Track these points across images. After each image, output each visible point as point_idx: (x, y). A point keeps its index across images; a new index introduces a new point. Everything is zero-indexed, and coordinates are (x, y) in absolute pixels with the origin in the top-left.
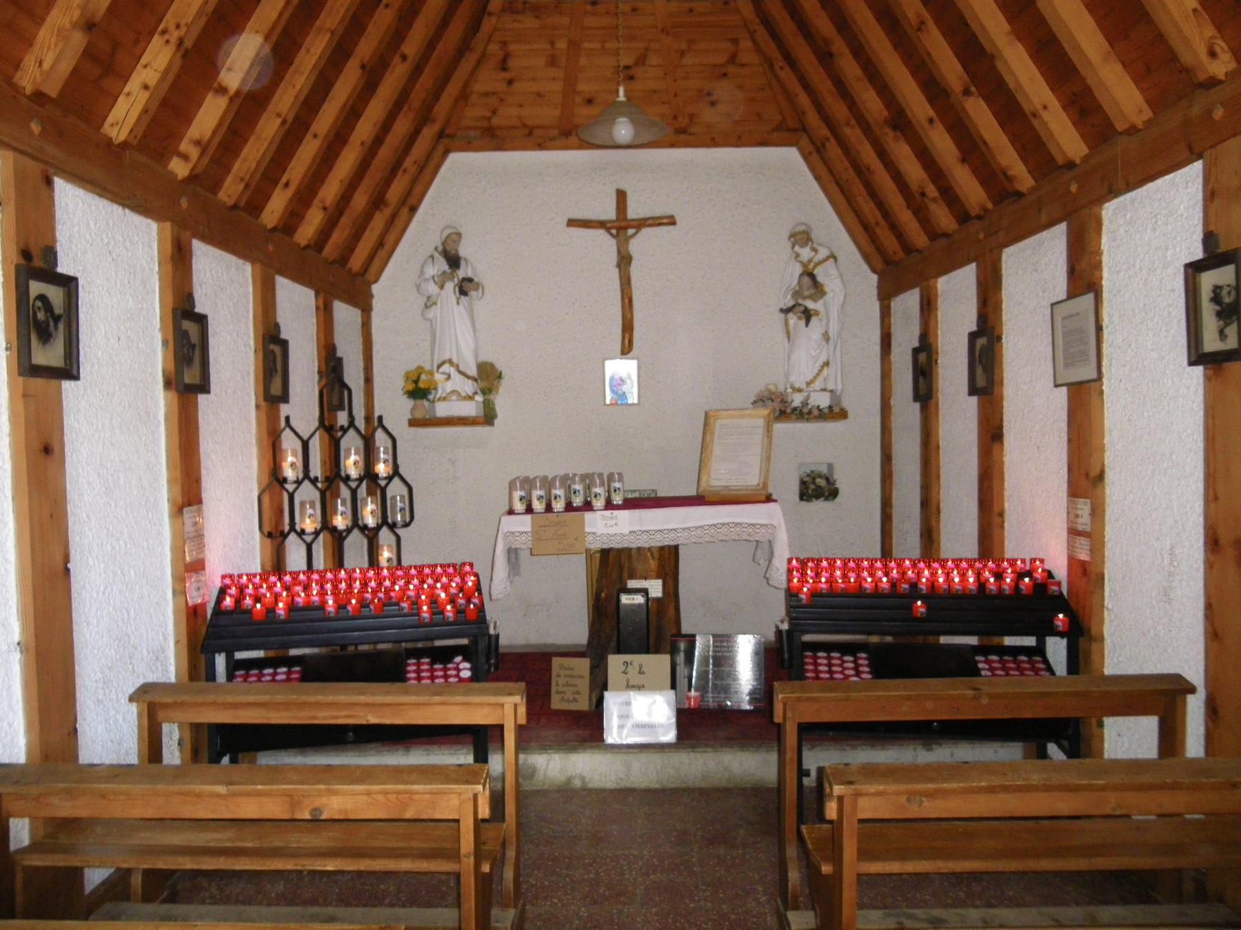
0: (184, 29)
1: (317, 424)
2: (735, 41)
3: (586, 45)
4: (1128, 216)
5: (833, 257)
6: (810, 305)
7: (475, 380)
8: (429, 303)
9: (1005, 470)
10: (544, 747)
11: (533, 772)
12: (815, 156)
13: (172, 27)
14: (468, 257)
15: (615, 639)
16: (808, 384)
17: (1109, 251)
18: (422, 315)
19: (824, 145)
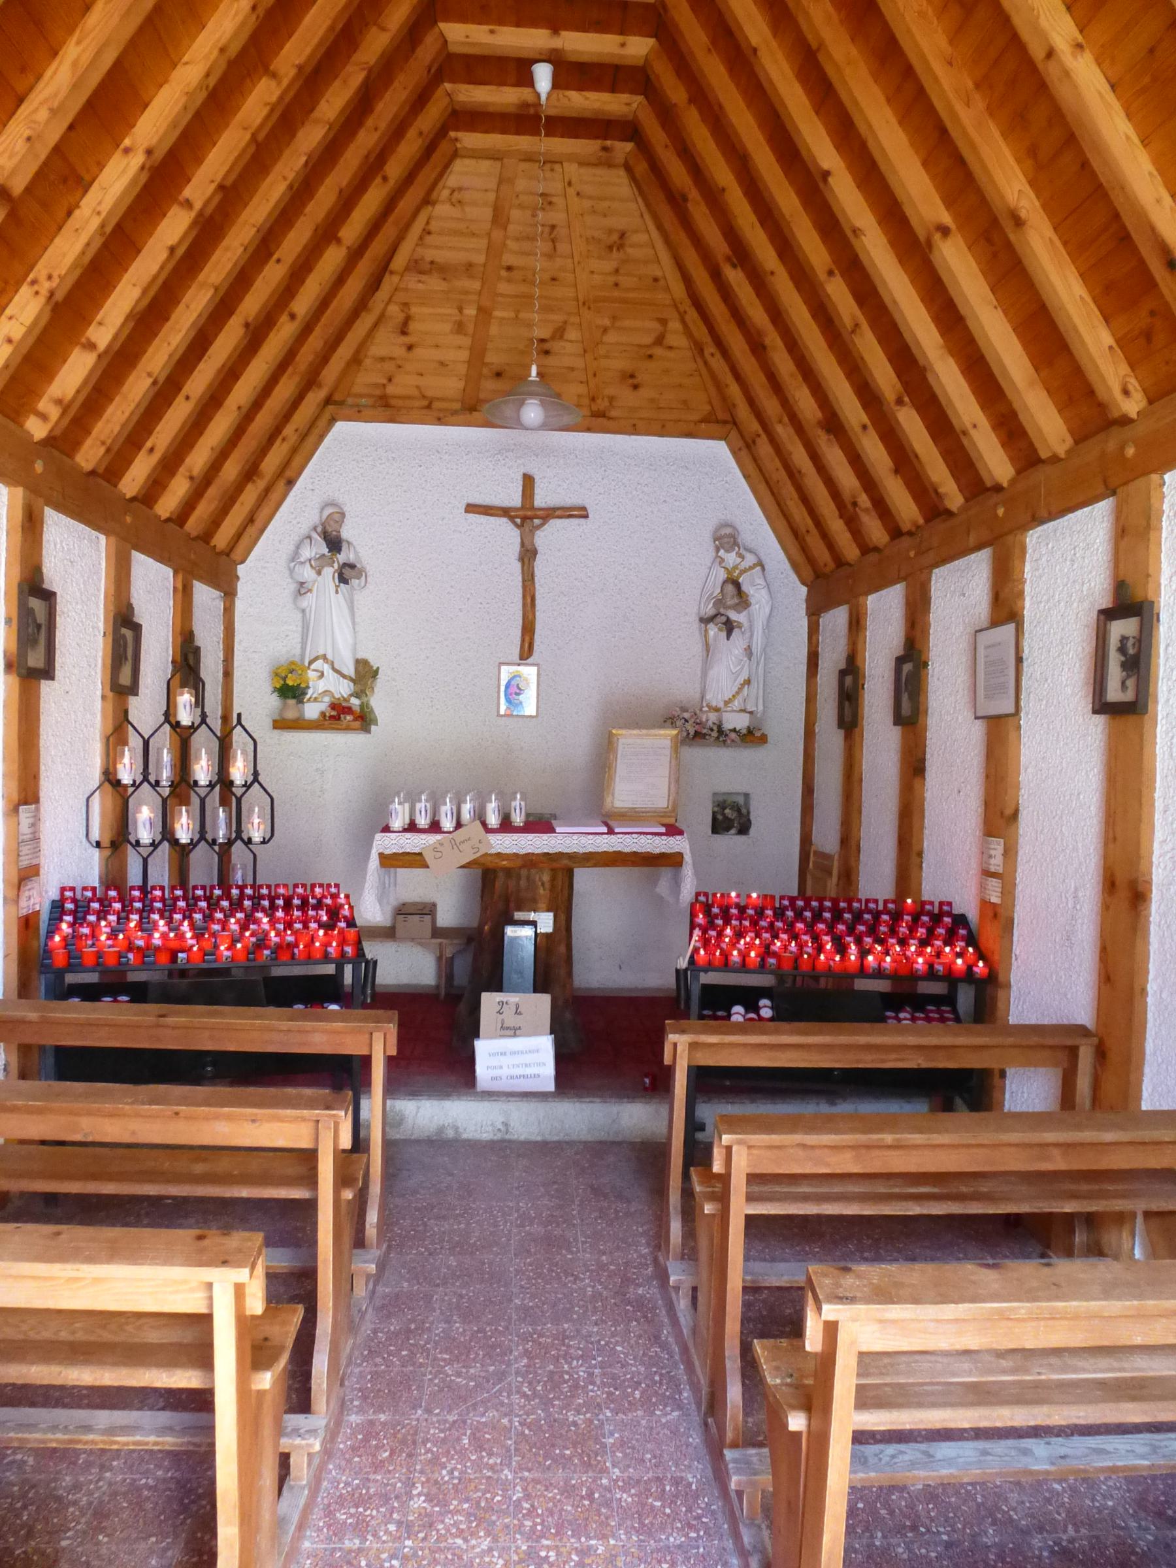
0: (56, 281)
1: (162, 719)
2: (663, 322)
4: (1050, 546)
5: (761, 564)
6: (733, 615)
7: (351, 680)
8: (302, 589)
9: (926, 807)
11: (400, 1121)
12: (744, 452)
13: (42, 278)
14: (350, 540)
16: (726, 703)
17: (1031, 581)
19: (754, 442)
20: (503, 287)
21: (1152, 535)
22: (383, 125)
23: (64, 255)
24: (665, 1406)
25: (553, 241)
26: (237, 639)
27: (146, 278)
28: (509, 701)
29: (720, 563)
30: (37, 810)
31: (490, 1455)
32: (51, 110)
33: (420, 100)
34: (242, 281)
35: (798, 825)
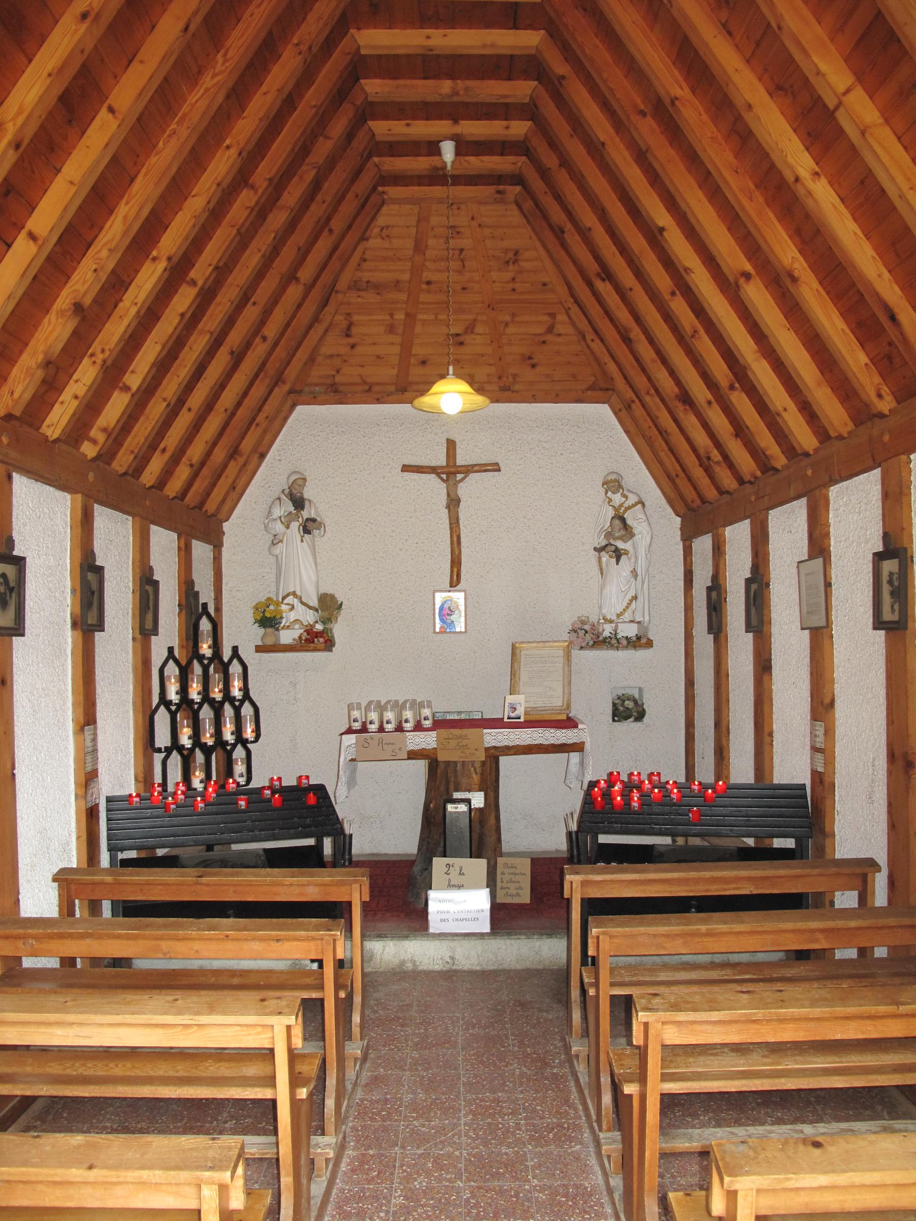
0: (107, 353)
2: (553, 315)
3: (420, 317)
6: (620, 545)
7: (317, 610)
8: (276, 541)
10: (380, 936)
12: (624, 413)
14: (311, 498)
15: (442, 844)
16: (618, 616)
18: (270, 553)
20: (423, 297)
21: (904, 499)
22: (329, 199)
23: (113, 334)
24: (571, 1142)
25: (462, 261)
26: (224, 581)
27: (165, 337)
28: (442, 620)
29: (609, 503)
30: (95, 729)
31: (447, 1173)
32: (110, 250)
33: (357, 174)
34: (230, 322)
35: (683, 712)
